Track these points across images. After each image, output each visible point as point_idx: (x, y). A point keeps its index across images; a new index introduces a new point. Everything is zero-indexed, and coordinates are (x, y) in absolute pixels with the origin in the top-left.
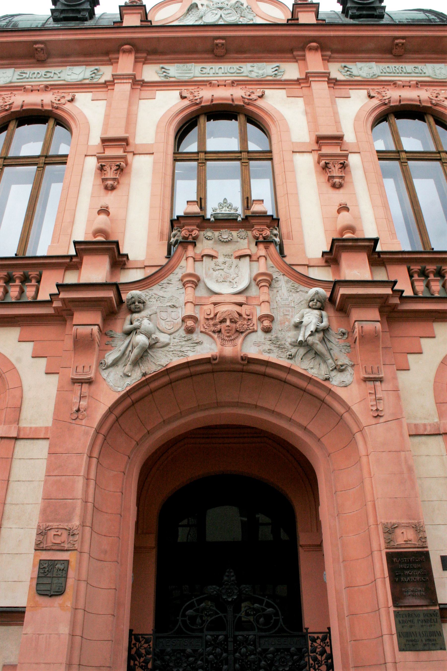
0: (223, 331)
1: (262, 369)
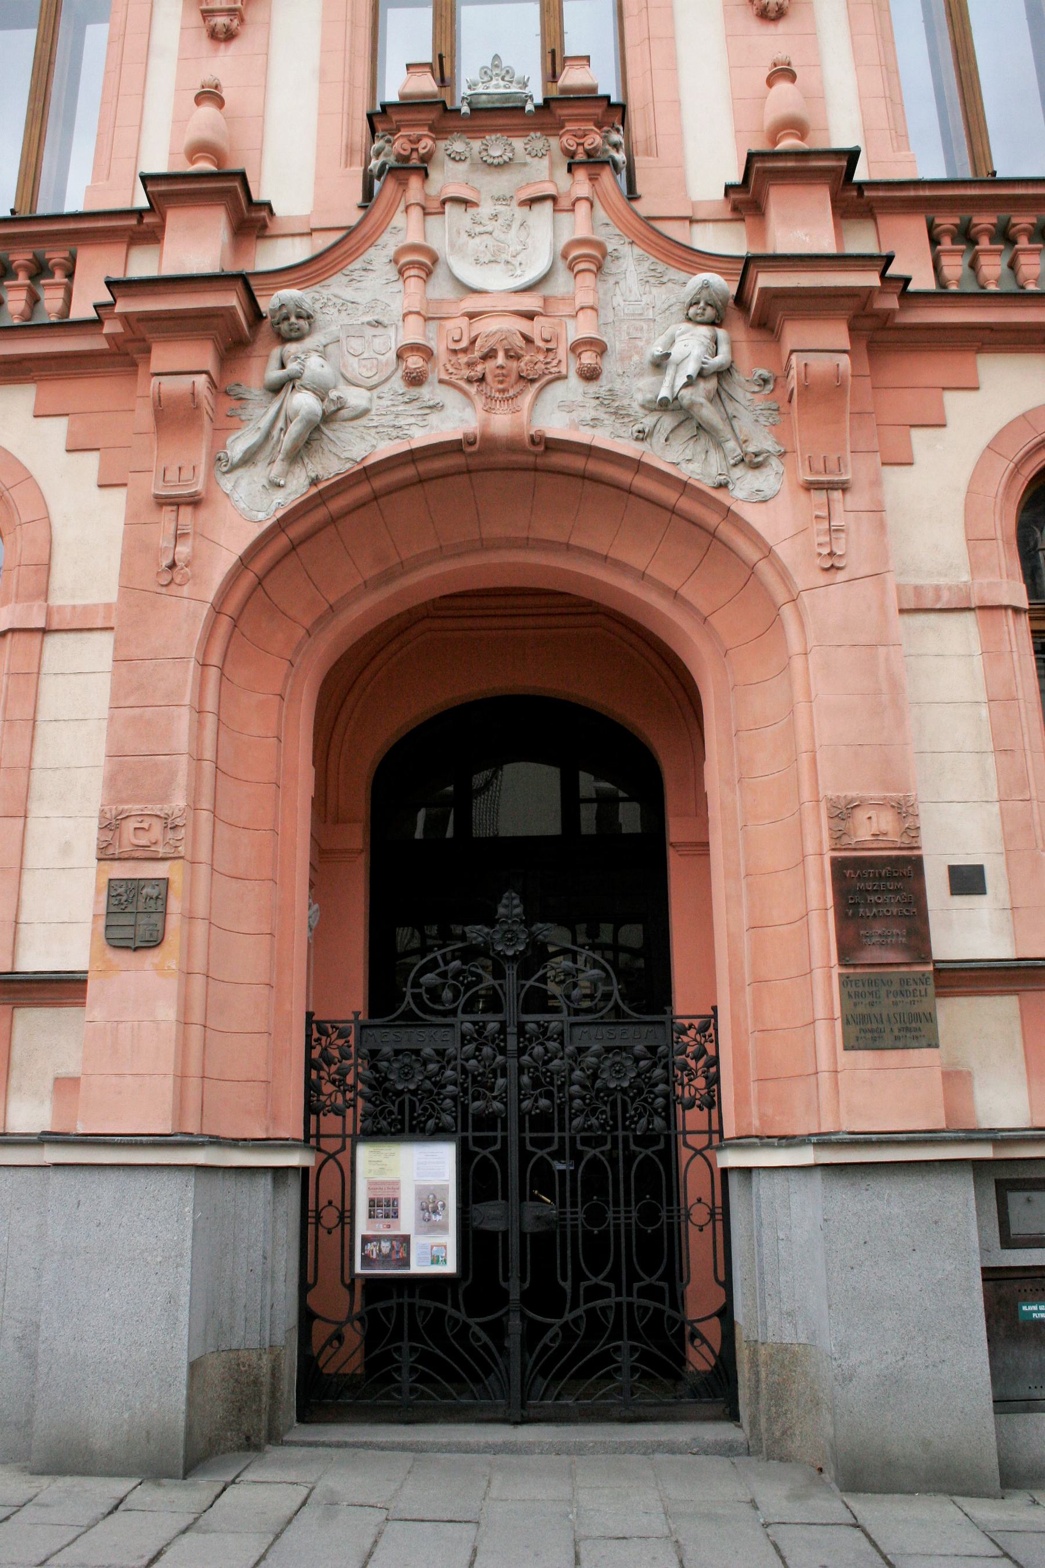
0: (489, 378)
1: (578, 463)
